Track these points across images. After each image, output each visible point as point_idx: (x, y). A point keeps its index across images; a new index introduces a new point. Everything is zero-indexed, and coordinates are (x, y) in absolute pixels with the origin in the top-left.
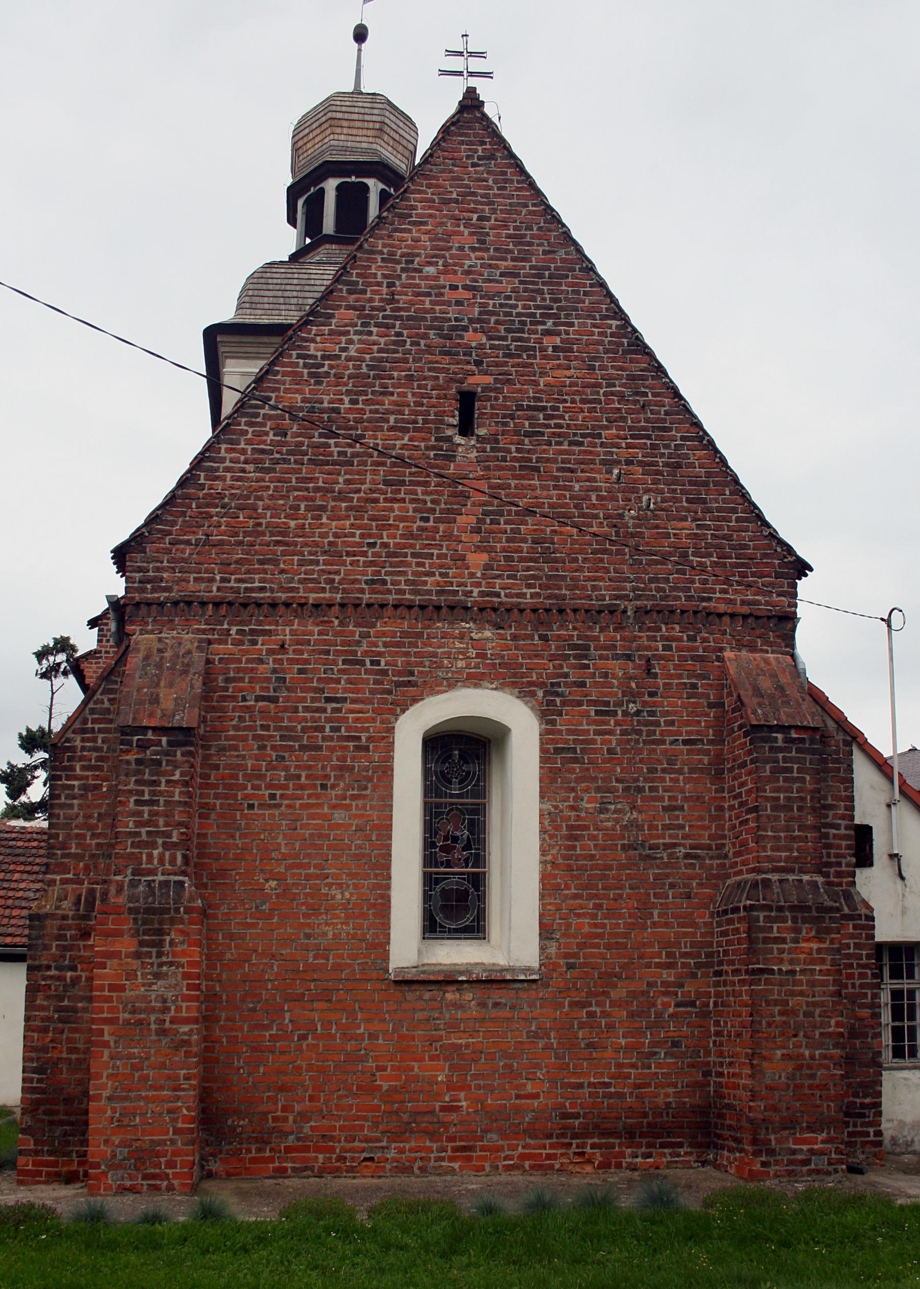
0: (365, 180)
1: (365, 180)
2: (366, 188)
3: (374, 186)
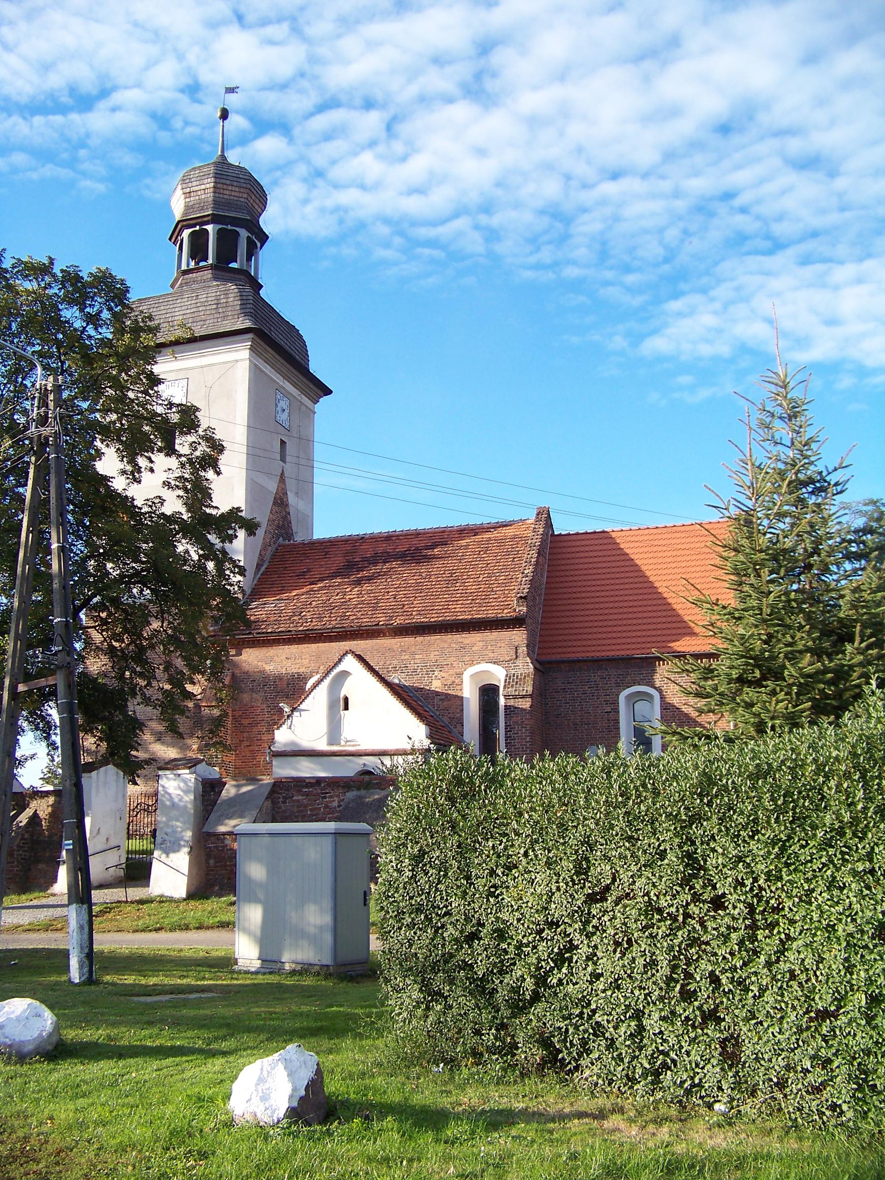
0: (237, 229)
1: (237, 229)
2: (238, 234)
3: (244, 234)
